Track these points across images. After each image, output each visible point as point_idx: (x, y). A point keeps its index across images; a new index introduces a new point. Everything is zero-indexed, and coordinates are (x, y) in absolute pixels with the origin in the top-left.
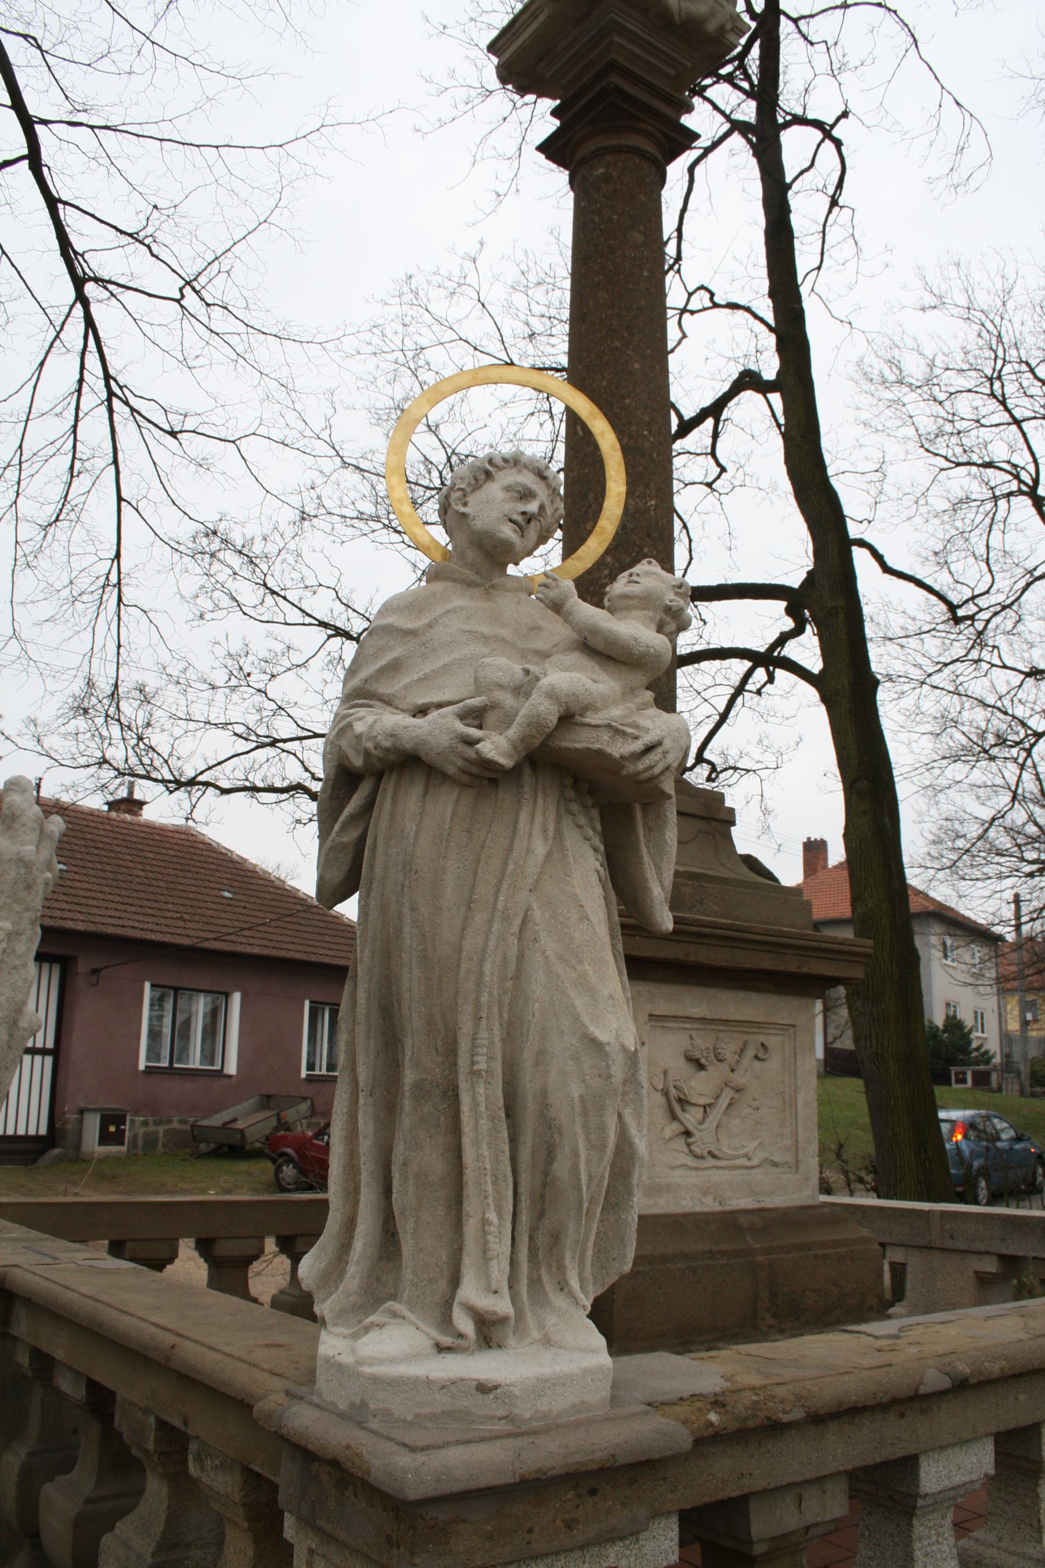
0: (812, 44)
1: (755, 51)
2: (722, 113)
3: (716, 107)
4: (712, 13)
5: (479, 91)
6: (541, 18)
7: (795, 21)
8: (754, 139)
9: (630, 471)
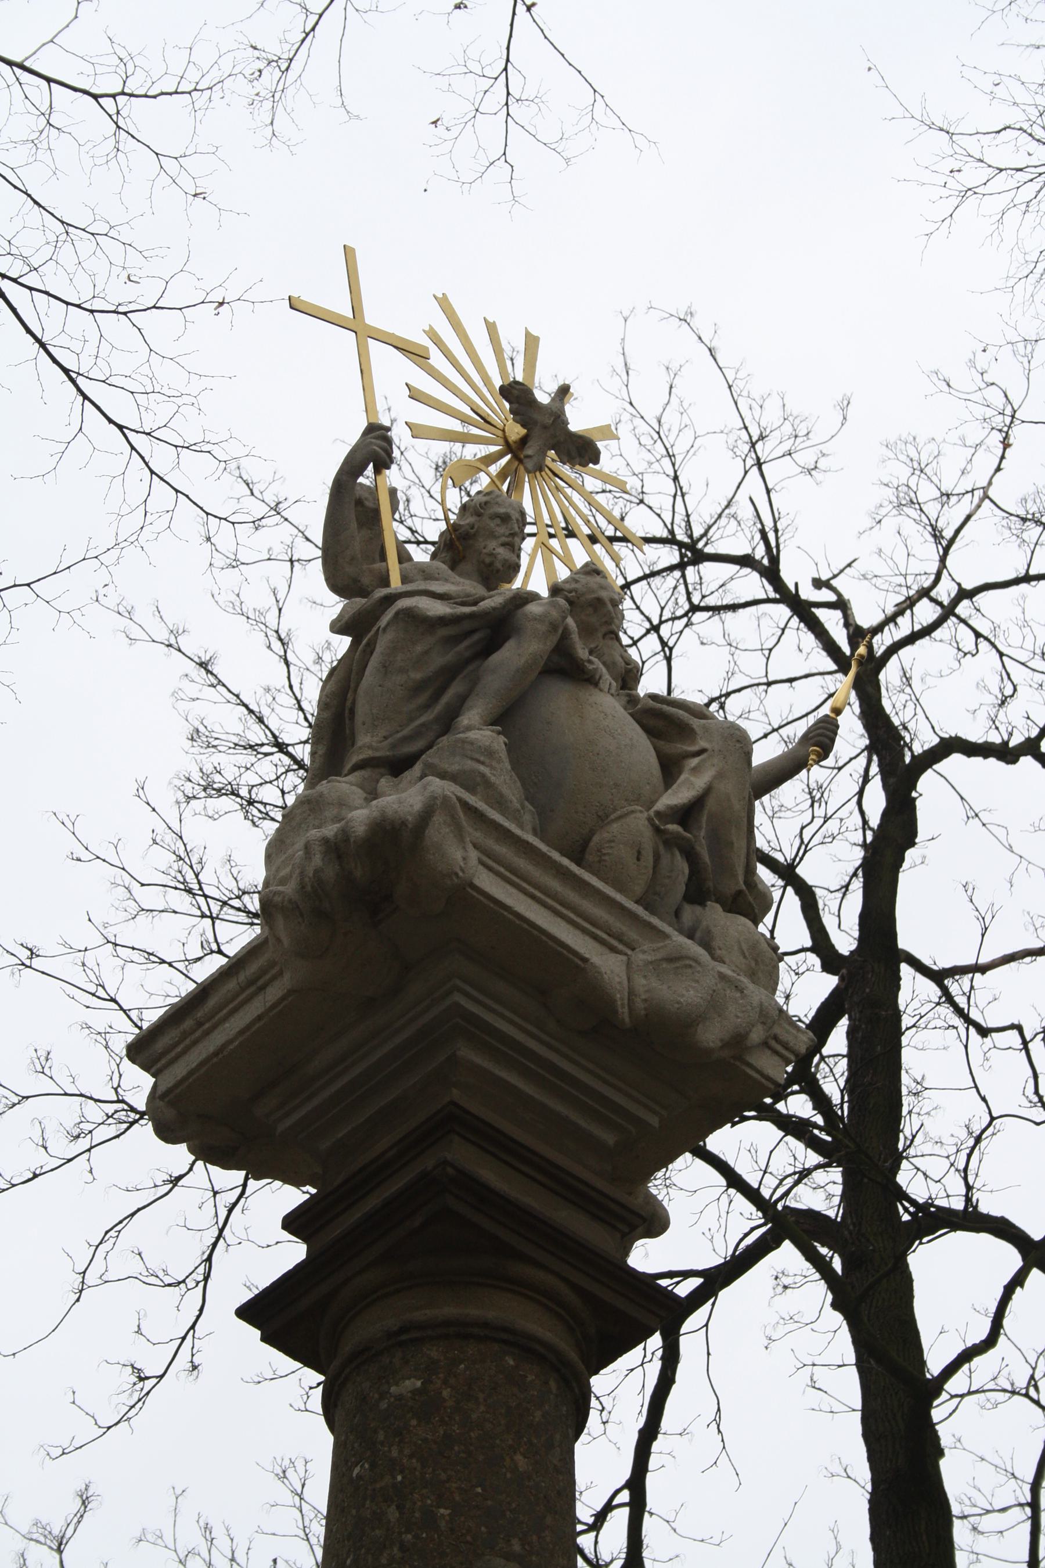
0: (984, 1032)
1: (838, 1041)
2: (752, 1195)
3: (734, 1180)
4: (715, 1005)
5: (110, 1108)
6: (274, 993)
7: (938, 977)
8: (837, 1264)
9: (640, 1230)
